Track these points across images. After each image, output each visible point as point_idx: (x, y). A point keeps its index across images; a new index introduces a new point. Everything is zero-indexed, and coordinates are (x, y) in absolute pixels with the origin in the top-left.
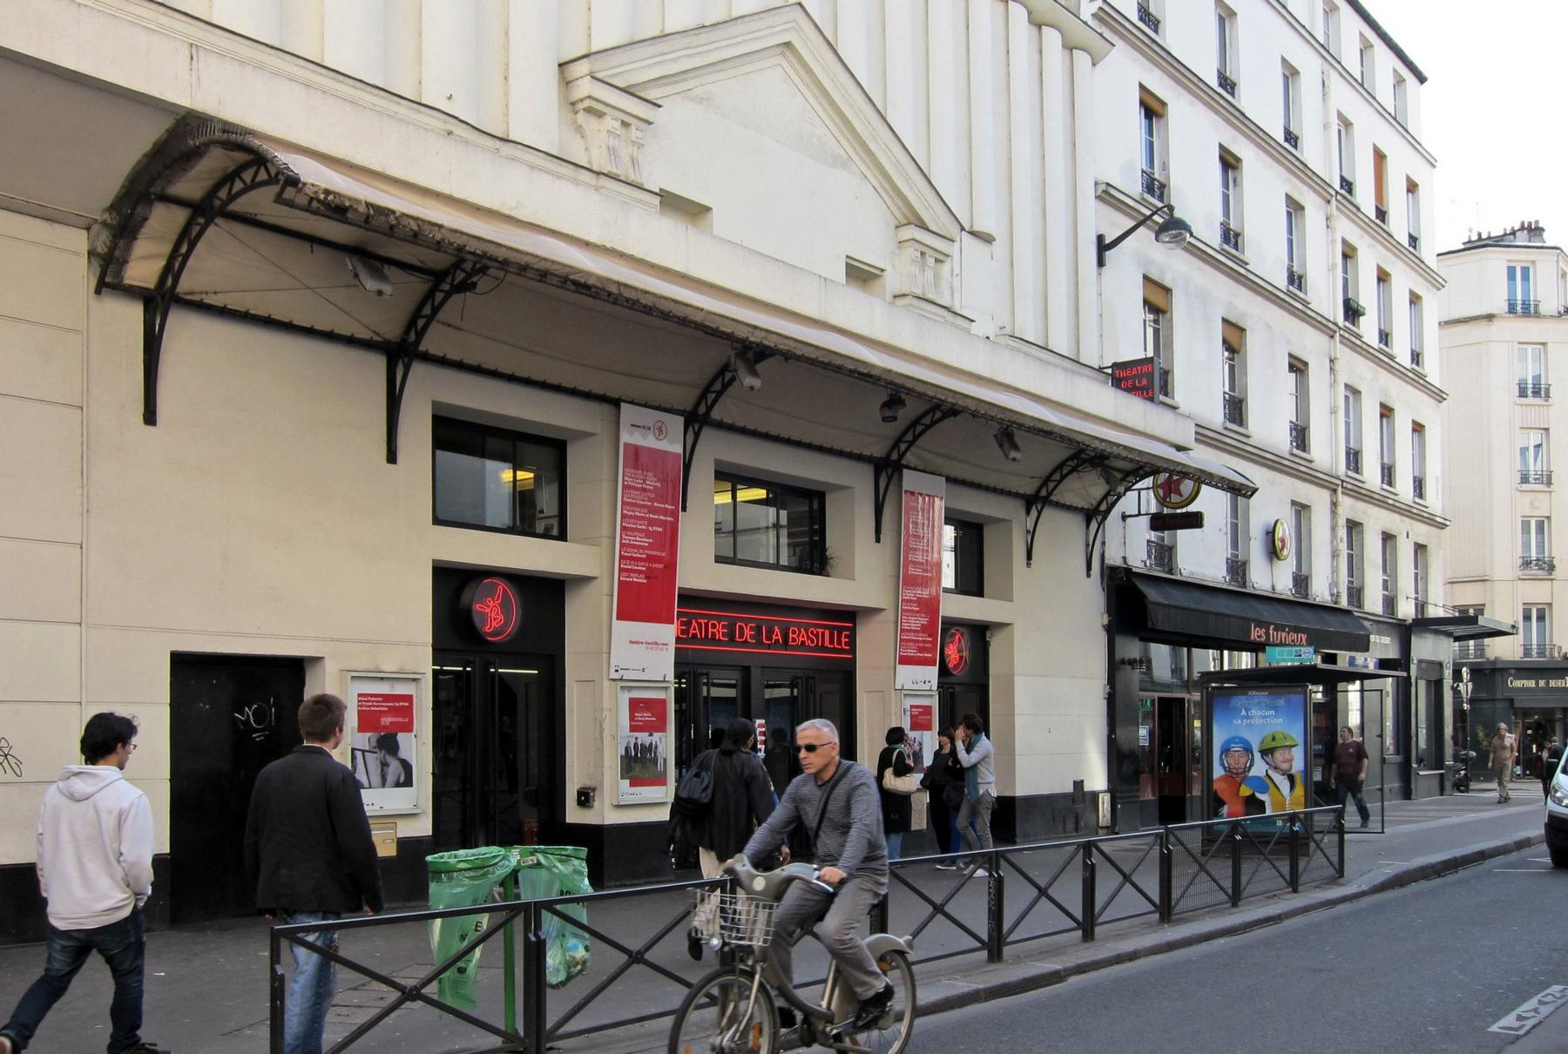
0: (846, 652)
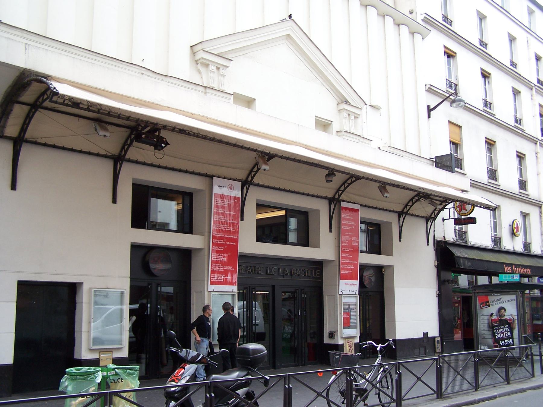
0: (319, 278)
